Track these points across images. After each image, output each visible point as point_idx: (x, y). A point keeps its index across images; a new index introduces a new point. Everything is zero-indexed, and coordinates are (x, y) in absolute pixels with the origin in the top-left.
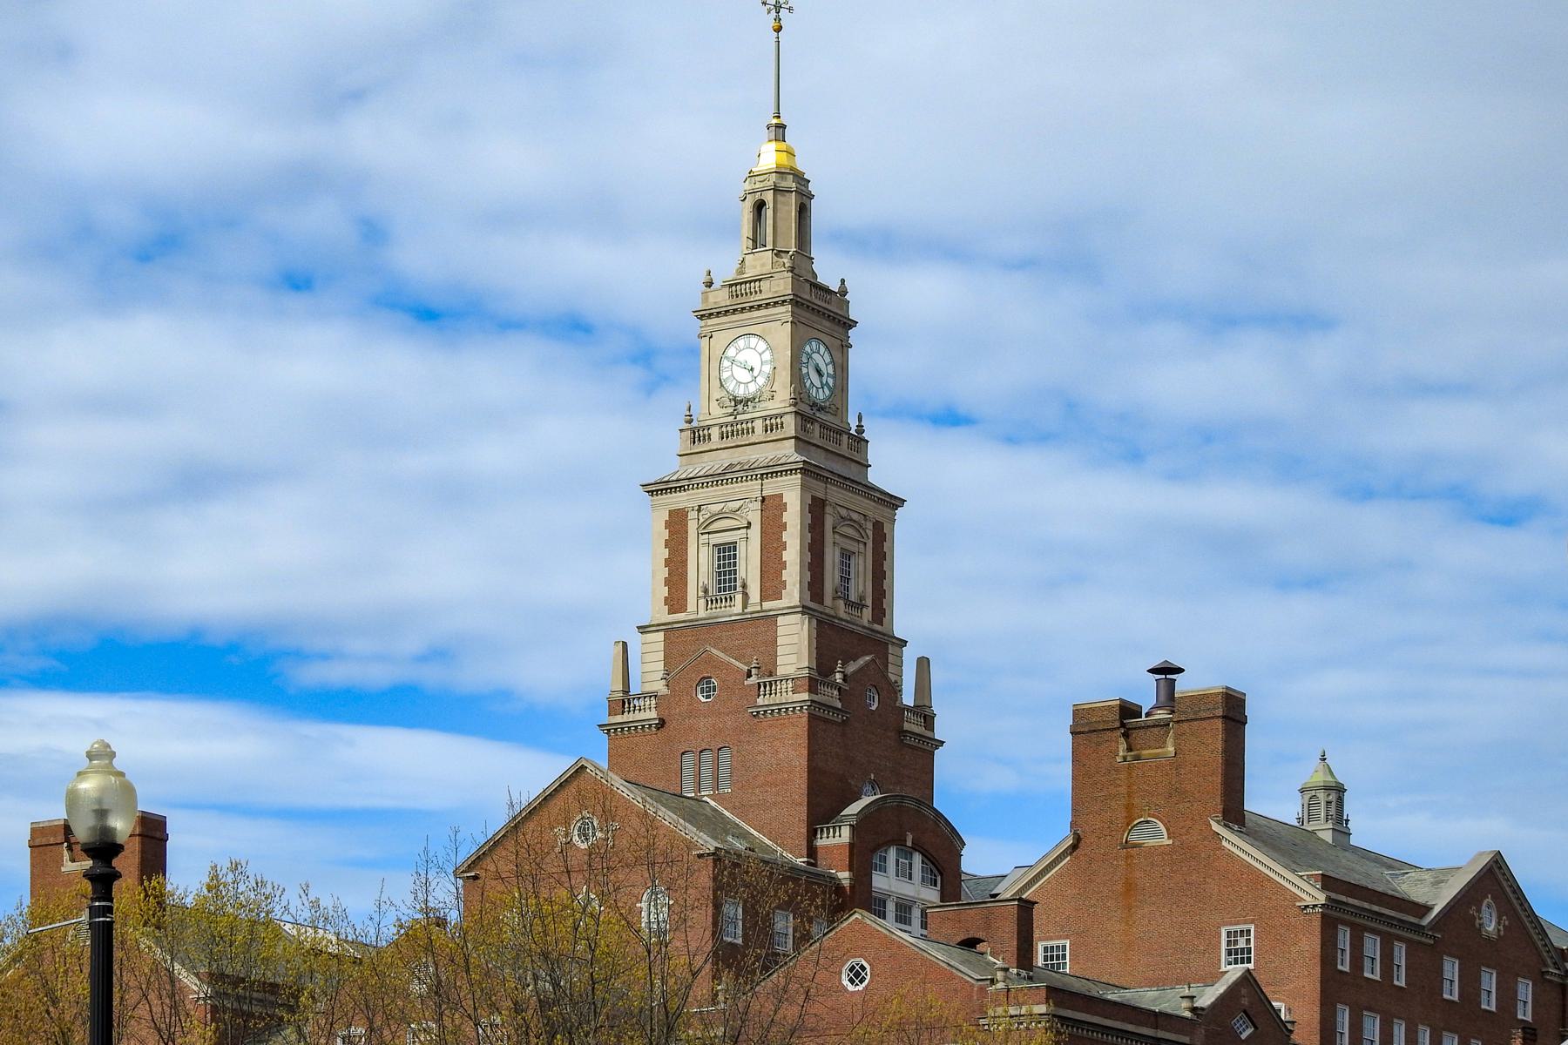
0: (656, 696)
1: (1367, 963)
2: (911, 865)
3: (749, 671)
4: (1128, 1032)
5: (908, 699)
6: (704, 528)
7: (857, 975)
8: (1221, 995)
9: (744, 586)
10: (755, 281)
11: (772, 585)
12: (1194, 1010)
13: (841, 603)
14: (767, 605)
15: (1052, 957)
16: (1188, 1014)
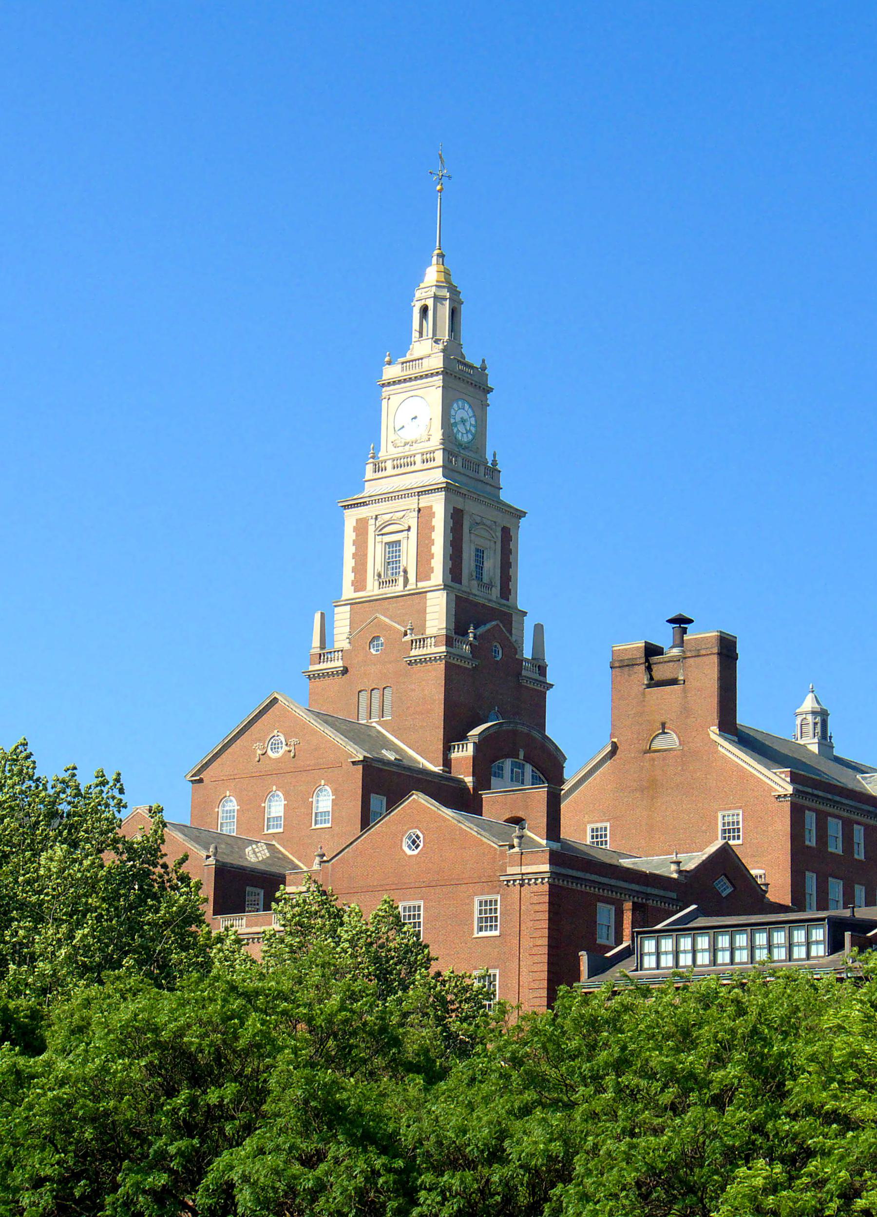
0: (342, 651)
1: (831, 841)
2: (523, 773)
3: (406, 631)
4: (621, 887)
5: (527, 653)
6: (380, 531)
7: (414, 842)
8: (703, 861)
9: (405, 571)
10: (418, 359)
11: (423, 573)
12: (680, 872)
13: (475, 583)
14: (420, 585)
15: (597, 836)
16: (675, 876)
